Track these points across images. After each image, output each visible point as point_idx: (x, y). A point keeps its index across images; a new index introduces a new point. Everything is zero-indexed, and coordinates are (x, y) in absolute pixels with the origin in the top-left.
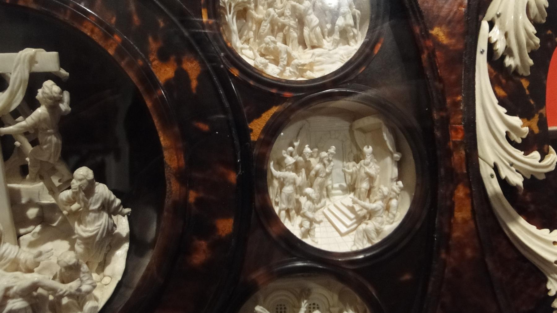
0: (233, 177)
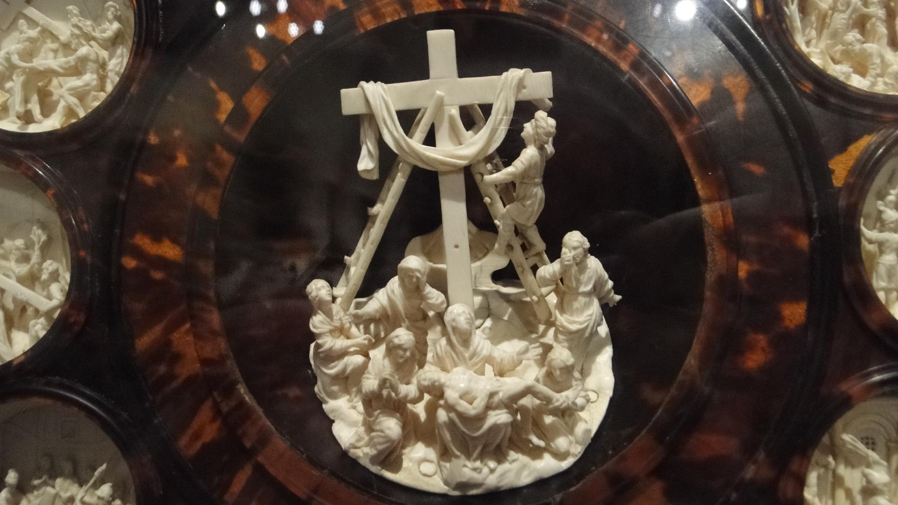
0: (803, 241)
